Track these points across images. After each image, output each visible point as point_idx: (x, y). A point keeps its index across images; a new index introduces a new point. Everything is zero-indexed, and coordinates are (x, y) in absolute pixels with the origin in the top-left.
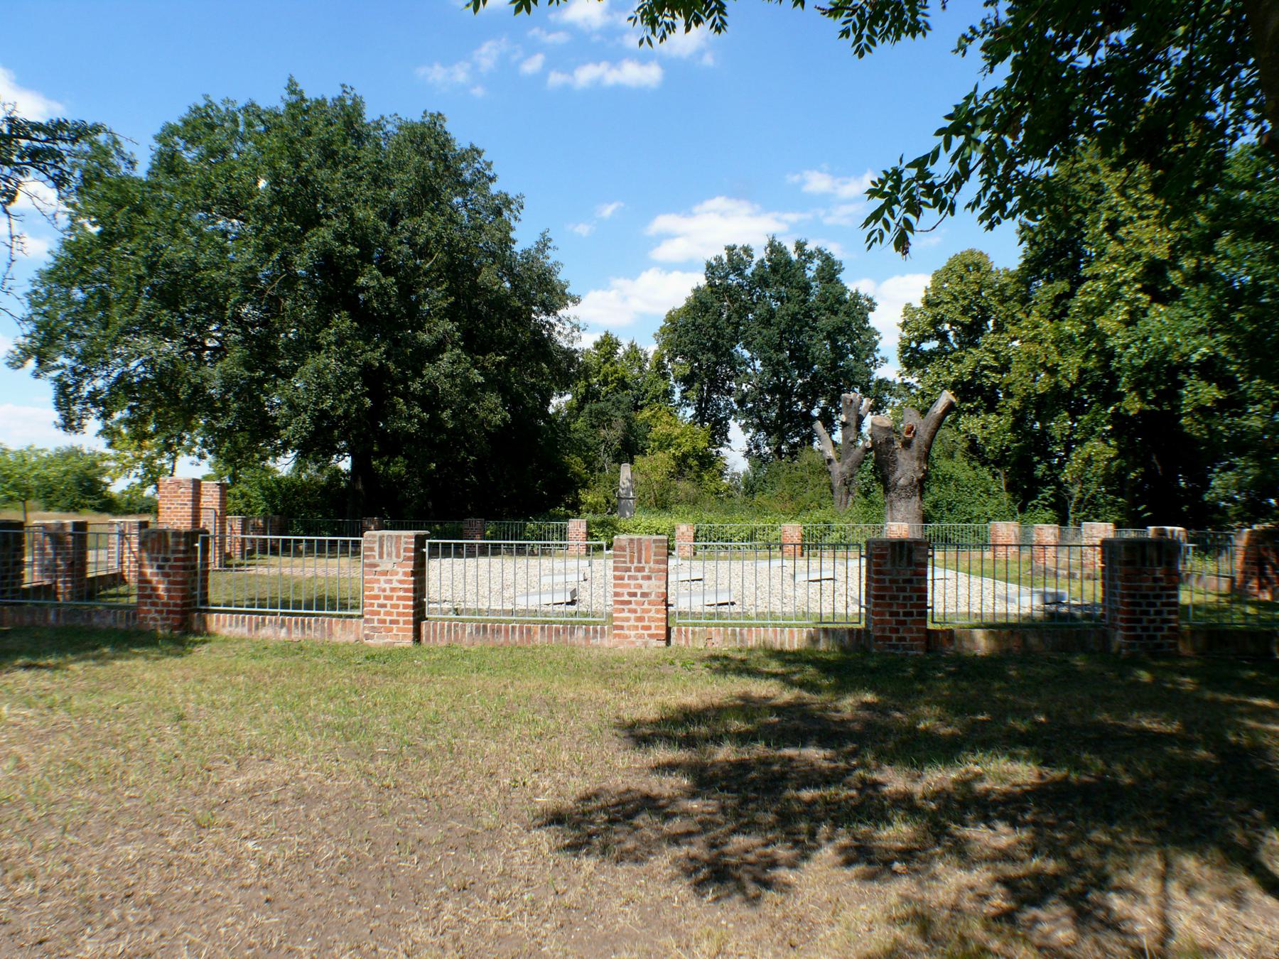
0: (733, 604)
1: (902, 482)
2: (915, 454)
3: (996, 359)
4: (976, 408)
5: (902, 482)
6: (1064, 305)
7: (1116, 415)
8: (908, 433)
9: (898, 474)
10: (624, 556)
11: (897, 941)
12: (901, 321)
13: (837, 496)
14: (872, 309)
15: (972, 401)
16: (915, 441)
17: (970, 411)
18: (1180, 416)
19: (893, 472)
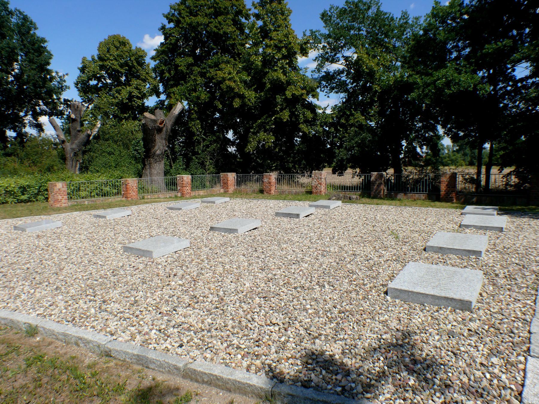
0: (277, 214)
1: (158, 152)
2: (164, 136)
3: (139, 93)
4: (129, 117)
5: (158, 152)
6: (191, 69)
7: (276, 122)
8: (161, 124)
9: (156, 148)
10: (368, 176)
11: (486, 386)
12: (81, 66)
13: (69, 163)
14: (51, 58)
15: (126, 114)
16: (164, 129)
17: (127, 119)
18: (299, 124)
19: (154, 146)
